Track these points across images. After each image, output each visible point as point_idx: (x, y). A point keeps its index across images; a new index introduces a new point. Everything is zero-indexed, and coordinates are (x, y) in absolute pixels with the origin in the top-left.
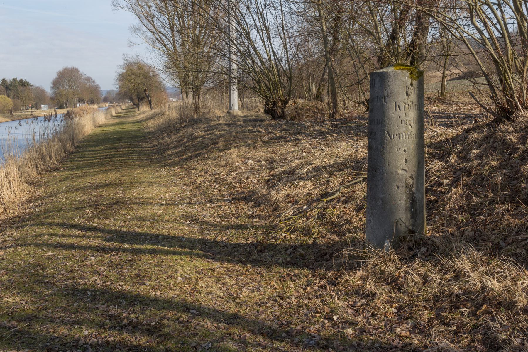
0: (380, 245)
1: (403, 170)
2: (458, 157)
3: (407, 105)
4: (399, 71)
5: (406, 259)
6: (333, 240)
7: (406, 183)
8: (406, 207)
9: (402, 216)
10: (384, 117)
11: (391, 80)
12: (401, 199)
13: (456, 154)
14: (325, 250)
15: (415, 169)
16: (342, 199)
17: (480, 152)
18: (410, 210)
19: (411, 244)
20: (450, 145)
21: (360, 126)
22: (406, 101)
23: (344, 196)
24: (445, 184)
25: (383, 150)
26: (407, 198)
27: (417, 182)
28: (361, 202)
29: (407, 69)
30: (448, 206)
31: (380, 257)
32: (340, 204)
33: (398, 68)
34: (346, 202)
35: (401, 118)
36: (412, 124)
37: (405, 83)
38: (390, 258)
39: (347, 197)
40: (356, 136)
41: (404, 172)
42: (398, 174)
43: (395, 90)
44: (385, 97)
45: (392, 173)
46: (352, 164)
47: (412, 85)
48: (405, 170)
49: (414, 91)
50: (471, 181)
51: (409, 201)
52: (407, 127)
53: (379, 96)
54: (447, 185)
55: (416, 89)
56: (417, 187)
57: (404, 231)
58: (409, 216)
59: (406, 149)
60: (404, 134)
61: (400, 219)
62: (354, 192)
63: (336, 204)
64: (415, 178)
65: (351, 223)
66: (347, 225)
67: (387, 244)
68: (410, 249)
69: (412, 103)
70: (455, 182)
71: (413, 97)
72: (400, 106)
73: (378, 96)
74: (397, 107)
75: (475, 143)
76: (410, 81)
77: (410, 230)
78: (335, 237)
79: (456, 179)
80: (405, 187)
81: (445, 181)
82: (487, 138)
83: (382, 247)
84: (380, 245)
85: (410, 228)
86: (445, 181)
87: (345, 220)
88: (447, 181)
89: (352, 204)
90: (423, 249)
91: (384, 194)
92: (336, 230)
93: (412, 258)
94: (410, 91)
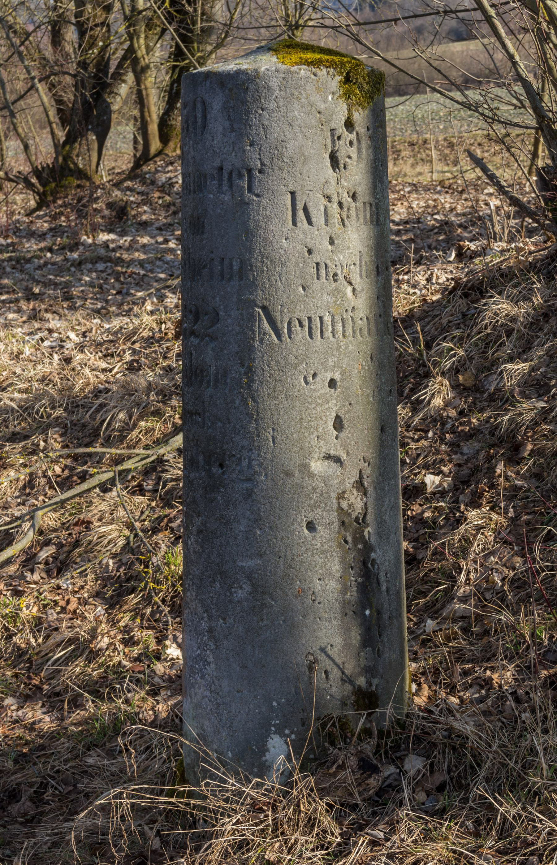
0: (252, 762)
1: (328, 457)
2: (455, 386)
3: (335, 205)
4: (304, 71)
5: (354, 807)
6: (31, 727)
7: (340, 509)
8: (344, 604)
9: (329, 638)
10: (250, 251)
11: (272, 105)
12: (323, 574)
13: (443, 374)
14: (10, 773)
15: (370, 454)
16: (43, 555)
17: (533, 369)
18: (359, 613)
19: (368, 748)
20: (415, 341)
21: (28, 261)
22: (331, 190)
23: (47, 543)
24: (430, 489)
25: (251, 381)
26: (347, 566)
27: (379, 501)
28: (120, 564)
29: (331, 64)
30: (462, 578)
31: (255, 808)
32: (36, 577)
33: (295, 57)
34: (59, 567)
35: (316, 257)
36: (356, 279)
37: (323, 118)
38: (297, 810)
39: (60, 546)
40: (28, 300)
41: (330, 468)
42: (312, 476)
43: (291, 147)
44: (250, 171)
45: (288, 474)
46: (59, 412)
47: (349, 125)
48: (337, 460)
49: (359, 150)
50: (524, 477)
51: (353, 578)
52: (337, 292)
53: (227, 167)
54: (440, 494)
55: (365, 143)
56: (380, 522)
57: (338, 696)
58: (356, 636)
59: (337, 376)
60: (327, 319)
61: (323, 650)
62: (87, 524)
63: (22, 577)
64: (370, 490)
65: (93, 655)
66: (81, 662)
67: (278, 751)
68: (367, 767)
69: (354, 197)
70: (466, 483)
71: (357, 174)
72: (311, 209)
73: (221, 169)
74: (301, 214)
75: (509, 333)
76: (341, 111)
77: (359, 693)
78: (39, 714)
79: (465, 471)
80: (336, 525)
81: (431, 481)
82: (546, 316)
83: (263, 769)
84: (252, 762)
85: (361, 681)
86: (431, 481)
87: (71, 641)
88: (437, 479)
89: (83, 574)
90: (414, 764)
91: (261, 555)
92: (36, 681)
93: (382, 803)
94: (345, 151)
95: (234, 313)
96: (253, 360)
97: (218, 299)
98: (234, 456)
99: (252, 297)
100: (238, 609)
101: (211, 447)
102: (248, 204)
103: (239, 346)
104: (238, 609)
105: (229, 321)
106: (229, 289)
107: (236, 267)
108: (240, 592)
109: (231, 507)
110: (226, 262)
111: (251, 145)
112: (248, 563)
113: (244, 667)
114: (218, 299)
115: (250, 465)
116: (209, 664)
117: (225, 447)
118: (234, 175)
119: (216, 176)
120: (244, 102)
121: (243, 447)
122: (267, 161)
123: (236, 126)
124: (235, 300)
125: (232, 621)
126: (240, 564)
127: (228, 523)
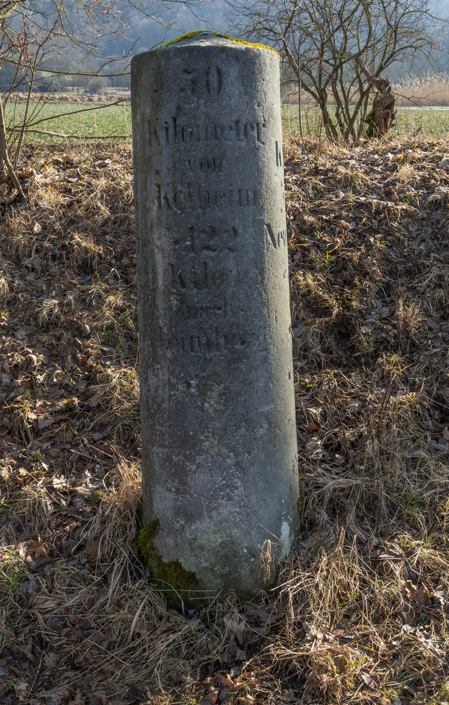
10: (260, 183)
25: (263, 278)
53: (243, 121)
73: (237, 122)
95: (250, 230)
96: (264, 263)
97: (237, 220)
98: (254, 334)
99: (262, 218)
100: (261, 442)
101: (234, 331)
102: (258, 149)
103: (255, 254)
104: (261, 442)
105: (247, 236)
106: (246, 212)
107: (251, 196)
108: (261, 430)
109: (253, 372)
110: (244, 192)
111: (258, 106)
112: (266, 409)
113: (267, 482)
114: (237, 220)
115: (265, 340)
116: (237, 488)
117: (247, 329)
118: (249, 127)
119: (234, 127)
120: (253, 73)
121: (260, 327)
122: (267, 118)
123: (248, 90)
124: (251, 220)
125: (256, 452)
126: (260, 410)
127: (251, 382)
